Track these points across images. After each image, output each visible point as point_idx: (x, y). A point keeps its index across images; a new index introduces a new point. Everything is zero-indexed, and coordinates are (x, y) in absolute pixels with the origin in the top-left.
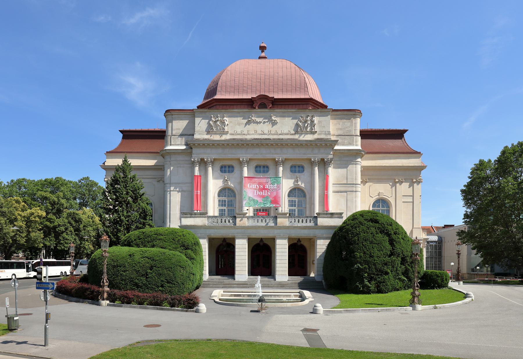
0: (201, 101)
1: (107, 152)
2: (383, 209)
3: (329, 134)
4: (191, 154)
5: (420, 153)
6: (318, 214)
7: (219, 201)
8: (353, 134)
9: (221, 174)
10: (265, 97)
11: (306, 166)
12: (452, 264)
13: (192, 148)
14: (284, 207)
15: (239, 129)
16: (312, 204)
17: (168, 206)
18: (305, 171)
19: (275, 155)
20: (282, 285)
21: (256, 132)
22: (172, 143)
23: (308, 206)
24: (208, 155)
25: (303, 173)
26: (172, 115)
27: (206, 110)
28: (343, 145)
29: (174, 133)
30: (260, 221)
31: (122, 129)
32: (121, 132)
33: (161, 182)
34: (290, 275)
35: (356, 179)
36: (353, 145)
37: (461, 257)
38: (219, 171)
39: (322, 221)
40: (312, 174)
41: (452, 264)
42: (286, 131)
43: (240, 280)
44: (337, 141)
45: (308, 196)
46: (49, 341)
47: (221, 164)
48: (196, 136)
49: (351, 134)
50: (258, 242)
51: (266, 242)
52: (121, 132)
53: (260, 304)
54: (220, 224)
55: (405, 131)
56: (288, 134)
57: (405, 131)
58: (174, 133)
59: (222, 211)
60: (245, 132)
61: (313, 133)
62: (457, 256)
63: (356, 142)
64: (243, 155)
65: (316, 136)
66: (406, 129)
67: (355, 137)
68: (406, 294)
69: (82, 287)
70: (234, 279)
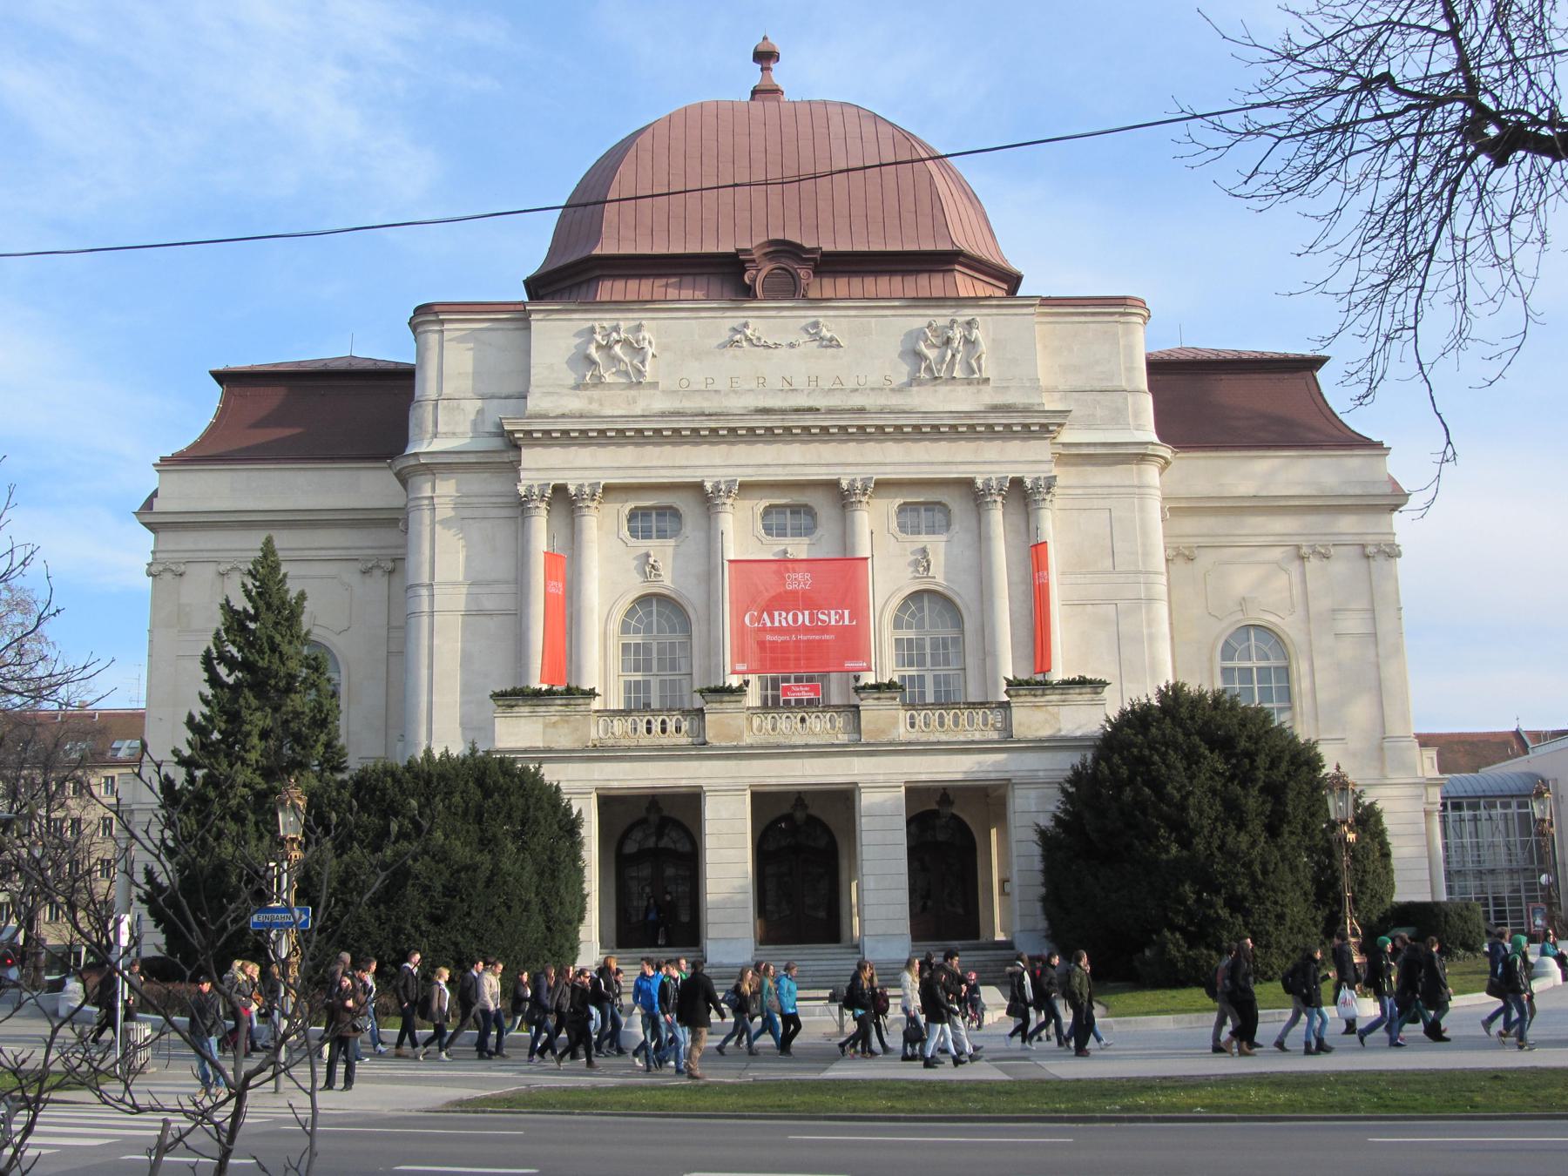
0: (534, 259)
1: (163, 459)
2: (1263, 664)
3: (1037, 389)
4: (514, 467)
5: (1379, 445)
6: (1014, 685)
7: (626, 647)
8: (1124, 384)
11: (957, 504)
14: (601, 667)
15: (696, 374)
16: (988, 653)
17: (424, 672)
19: (839, 470)
21: (762, 380)
22: (441, 428)
23: (971, 661)
26: (442, 322)
28: (1089, 427)
29: (448, 389)
31: (220, 367)
32: (220, 377)
35: (1146, 554)
36: (1126, 427)
39: (1032, 719)
40: (981, 539)
42: (874, 379)
43: (726, 960)
44: (1065, 413)
45: (969, 625)
47: (632, 505)
48: (534, 403)
49: (1115, 383)
50: (786, 809)
51: (814, 811)
52: (220, 377)
54: (646, 740)
55: (1319, 362)
57: (1319, 362)
58: (448, 389)
59: (637, 690)
61: (974, 379)
63: (1137, 415)
64: (708, 464)
65: (987, 397)
67: (1130, 398)
69: (571, 827)
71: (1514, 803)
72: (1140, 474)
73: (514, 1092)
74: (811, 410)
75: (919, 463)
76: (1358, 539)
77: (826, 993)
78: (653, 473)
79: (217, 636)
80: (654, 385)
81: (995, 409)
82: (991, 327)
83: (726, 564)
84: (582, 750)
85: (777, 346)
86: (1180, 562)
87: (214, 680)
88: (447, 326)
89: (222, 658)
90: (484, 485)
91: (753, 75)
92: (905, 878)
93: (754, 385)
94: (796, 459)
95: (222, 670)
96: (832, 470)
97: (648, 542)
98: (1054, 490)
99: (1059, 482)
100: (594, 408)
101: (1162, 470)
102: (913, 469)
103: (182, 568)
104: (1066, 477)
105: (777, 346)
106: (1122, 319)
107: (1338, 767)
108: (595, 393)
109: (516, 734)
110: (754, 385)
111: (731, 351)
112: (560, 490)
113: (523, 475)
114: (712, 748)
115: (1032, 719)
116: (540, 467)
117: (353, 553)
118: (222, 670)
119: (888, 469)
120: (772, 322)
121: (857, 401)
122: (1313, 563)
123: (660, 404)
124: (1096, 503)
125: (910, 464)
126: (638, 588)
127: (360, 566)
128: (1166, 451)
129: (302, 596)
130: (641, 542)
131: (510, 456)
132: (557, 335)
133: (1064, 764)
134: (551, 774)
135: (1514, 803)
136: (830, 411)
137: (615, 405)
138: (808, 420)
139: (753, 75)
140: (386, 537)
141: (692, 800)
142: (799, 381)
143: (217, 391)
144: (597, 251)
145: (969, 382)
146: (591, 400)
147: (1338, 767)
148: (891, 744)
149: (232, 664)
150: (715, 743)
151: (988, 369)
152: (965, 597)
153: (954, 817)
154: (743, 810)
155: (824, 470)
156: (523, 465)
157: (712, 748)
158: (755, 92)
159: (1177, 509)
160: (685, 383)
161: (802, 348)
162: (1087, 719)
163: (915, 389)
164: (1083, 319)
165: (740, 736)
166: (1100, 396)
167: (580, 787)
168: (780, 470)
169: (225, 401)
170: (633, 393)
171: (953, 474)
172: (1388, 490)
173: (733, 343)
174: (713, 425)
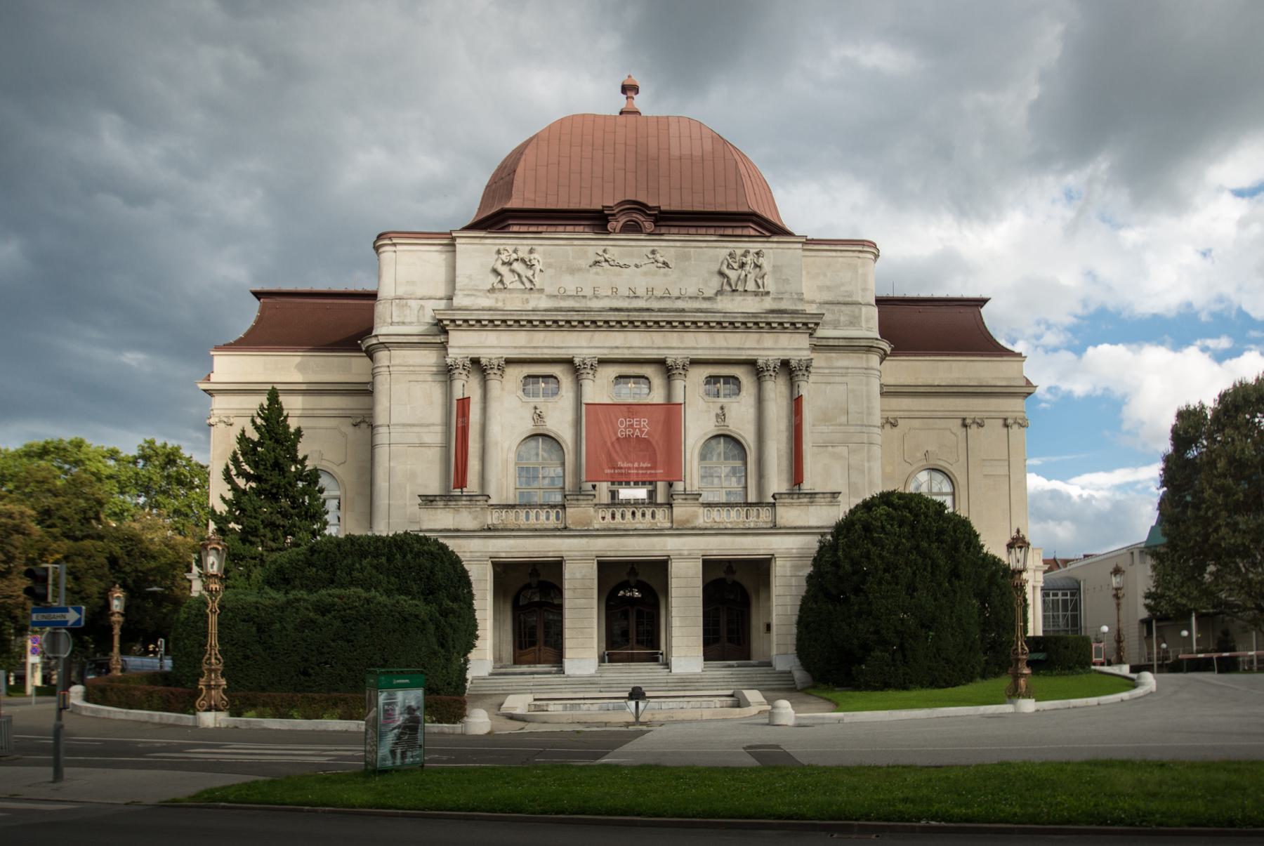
4: (444, 346)
5: (1020, 355)
8: (860, 300)
9: (525, 399)
10: (641, 207)
12: (1105, 629)
13: (446, 332)
15: (570, 284)
18: (743, 393)
20: (686, 683)
21: (615, 290)
24: (492, 345)
25: (738, 398)
27: (482, 234)
30: (628, 515)
33: (364, 426)
34: (707, 657)
35: (869, 414)
37: (1122, 601)
38: (520, 393)
41: (1105, 629)
42: (692, 291)
43: (578, 673)
46: (67, 771)
49: (854, 299)
52: (258, 295)
53: (633, 703)
55: (982, 302)
56: (697, 298)
57: (982, 302)
60: (588, 291)
61: (761, 293)
62: (1113, 602)
65: (768, 304)
66: (985, 296)
68: (1005, 682)
70: (561, 671)
71: (1060, 593)
72: (867, 360)
73: (249, 786)
74: (648, 310)
75: (720, 348)
76: (1004, 415)
77: (626, 695)
78: (539, 351)
79: (235, 459)
80: (541, 291)
81: (773, 311)
82: (771, 252)
83: (584, 407)
84: (483, 530)
85: (626, 266)
86: (888, 427)
87: (235, 488)
88: (399, 248)
89: (242, 473)
90: (429, 358)
91: (621, 102)
92: (701, 619)
93: (609, 293)
94: (636, 344)
95: (241, 482)
96: (661, 352)
97: (537, 400)
98: (811, 369)
99: (814, 364)
100: (500, 305)
101: (882, 360)
102: (717, 352)
103: (232, 420)
104: (819, 360)
105: (626, 266)
106: (861, 255)
107: (1018, 531)
108: (501, 296)
109: (437, 521)
110: (609, 293)
111: (595, 269)
112: (475, 362)
113: (450, 351)
114: (571, 530)
115: (790, 515)
116: (462, 344)
117: (348, 413)
118: (241, 482)
119: (700, 352)
120: (621, 248)
121: (680, 304)
122: (973, 430)
123: (544, 303)
124: (838, 379)
125: (714, 348)
126: (528, 427)
127: (350, 420)
128: (885, 346)
129: (299, 432)
130: (531, 399)
131: (442, 338)
132: (479, 255)
133: (813, 543)
134: (452, 544)
135: (1060, 593)
136: (660, 310)
137: (514, 303)
138: (645, 316)
139: (621, 102)
140: (366, 399)
141: (556, 566)
142: (641, 291)
143: (256, 305)
144: (509, 206)
145: (756, 294)
146: (497, 300)
147: (1018, 531)
148: (693, 529)
149: (249, 478)
150: (572, 527)
151: (770, 284)
152: (749, 438)
153: (736, 583)
154: (590, 573)
155: (656, 351)
156: (451, 343)
157: (571, 530)
158: (621, 113)
159: (886, 392)
160: (562, 291)
161: (643, 269)
162: (827, 516)
163: (719, 298)
164: (834, 254)
165: (589, 524)
166: (843, 308)
167: (478, 559)
168: (626, 351)
169: (262, 311)
170: (526, 296)
171: (744, 355)
172: (1023, 383)
173: (597, 263)
174: (580, 318)
